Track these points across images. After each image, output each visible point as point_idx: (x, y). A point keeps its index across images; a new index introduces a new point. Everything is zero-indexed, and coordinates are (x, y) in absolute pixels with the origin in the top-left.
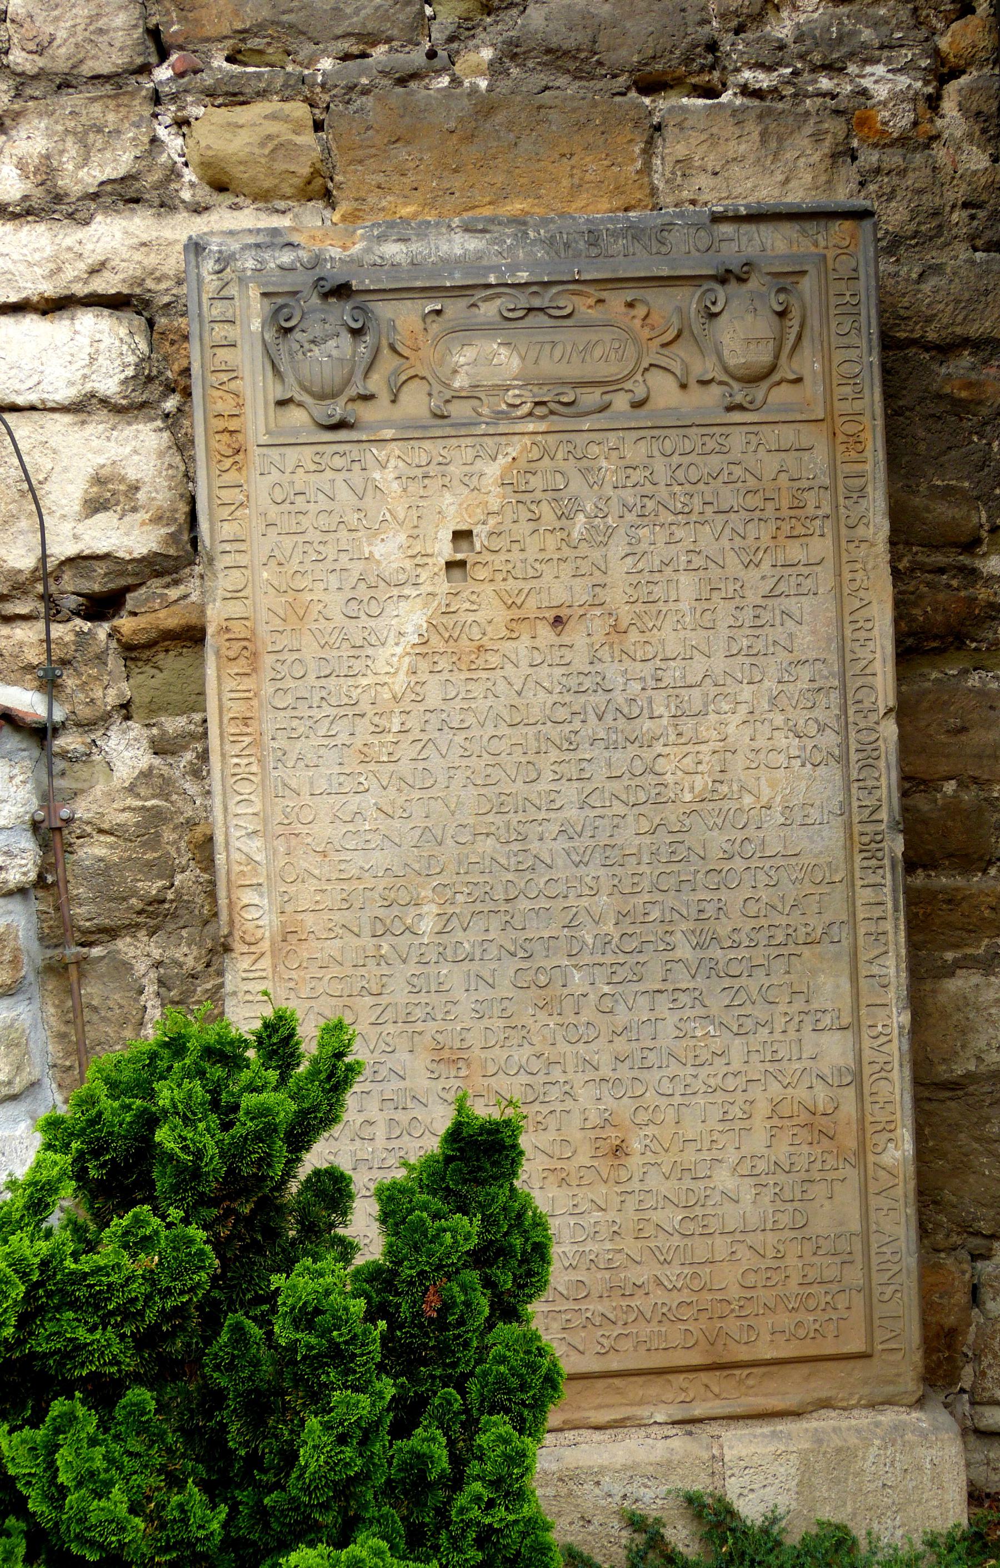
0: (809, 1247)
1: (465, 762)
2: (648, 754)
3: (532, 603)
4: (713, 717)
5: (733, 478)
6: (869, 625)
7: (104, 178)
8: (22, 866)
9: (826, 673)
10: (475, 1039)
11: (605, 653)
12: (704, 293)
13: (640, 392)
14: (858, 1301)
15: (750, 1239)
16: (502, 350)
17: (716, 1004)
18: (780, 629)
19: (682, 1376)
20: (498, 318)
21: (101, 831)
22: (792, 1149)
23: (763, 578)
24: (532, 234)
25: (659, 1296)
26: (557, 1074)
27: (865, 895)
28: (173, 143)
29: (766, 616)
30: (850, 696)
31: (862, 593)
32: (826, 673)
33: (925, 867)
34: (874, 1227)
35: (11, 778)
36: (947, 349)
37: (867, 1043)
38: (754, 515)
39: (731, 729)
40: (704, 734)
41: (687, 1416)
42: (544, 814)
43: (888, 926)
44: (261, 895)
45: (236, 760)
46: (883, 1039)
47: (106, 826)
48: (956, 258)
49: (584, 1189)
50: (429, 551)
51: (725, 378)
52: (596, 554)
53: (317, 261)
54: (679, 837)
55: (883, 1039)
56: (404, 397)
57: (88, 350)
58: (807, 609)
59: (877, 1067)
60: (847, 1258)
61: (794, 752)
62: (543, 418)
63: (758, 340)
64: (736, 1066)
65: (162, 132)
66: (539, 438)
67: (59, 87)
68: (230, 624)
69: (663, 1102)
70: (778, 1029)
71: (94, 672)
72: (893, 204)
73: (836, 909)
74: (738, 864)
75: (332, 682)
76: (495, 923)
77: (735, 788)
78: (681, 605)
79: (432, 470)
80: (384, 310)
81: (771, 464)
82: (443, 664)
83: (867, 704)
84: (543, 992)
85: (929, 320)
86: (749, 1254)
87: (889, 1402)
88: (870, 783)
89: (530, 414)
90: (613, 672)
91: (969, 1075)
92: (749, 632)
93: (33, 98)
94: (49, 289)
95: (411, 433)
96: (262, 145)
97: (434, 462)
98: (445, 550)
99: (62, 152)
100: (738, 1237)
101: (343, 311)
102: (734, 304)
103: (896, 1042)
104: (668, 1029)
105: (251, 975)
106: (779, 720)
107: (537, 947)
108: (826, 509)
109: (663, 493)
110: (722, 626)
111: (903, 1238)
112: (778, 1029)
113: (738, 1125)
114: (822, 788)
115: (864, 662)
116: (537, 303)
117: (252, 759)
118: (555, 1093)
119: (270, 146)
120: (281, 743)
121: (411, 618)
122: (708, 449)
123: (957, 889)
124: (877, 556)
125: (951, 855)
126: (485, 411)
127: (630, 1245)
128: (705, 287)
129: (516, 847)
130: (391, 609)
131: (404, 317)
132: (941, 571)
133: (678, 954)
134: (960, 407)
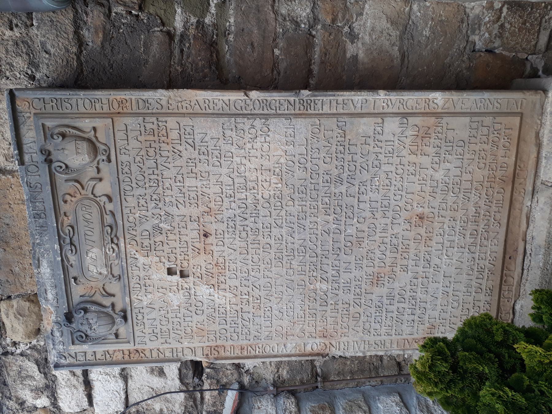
0: (473, 140)
1: (262, 272)
2: (262, 201)
3: (197, 245)
4: (247, 174)
5: (141, 161)
6: (207, 101)
7: (38, 372)
8: (290, 404)
9: (228, 124)
10: (370, 270)
11: (219, 217)
12: (57, 171)
13: (105, 199)
14: (498, 119)
15: (465, 165)
16: (90, 255)
17: (366, 176)
18: (209, 143)
19: (514, 193)
20: (76, 255)
21: (278, 371)
22: (431, 146)
23: (186, 150)
24: (38, 241)
25: (482, 203)
26: (387, 240)
27: (326, 109)
28: (22, 347)
29: (203, 149)
30: (238, 112)
31: (192, 104)
32: (228, 124)
33: (310, 65)
34: (469, 111)
35: (259, 408)
36: (81, 42)
37: (390, 110)
38: (158, 152)
39: (252, 167)
40: (254, 178)
41: (531, 193)
42: (284, 242)
43: (340, 99)
44: (308, 343)
45: (257, 352)
46: (389, 103)
47: (276, 370)
48: (37, 35)
49: (435, 231)
50: (176, 284)
51: (96, 162)
52: (177, 219)
53: (57, 323)
54: (296, 189)
55: (389, 103)
56: (111, 291)
57: (104, 376)
58: (200, 131)
59: (401, 106)
60: (480, 123)
61: (263, 140)
62: (118, 239)
63: (77, 148)
64: (393, 169)
65: (18, 351)
66: (127, 241)
67: (5, 385)
68: (205, 354)
69: (404, 199)
70: (379, 150)
71: (221, 373)
72: (14, 64)
73: (331, 123)
74: (309, 165)
75: (228, 320)
76: (325, 261)
77: (277, 166)
78: (199, 186)
79: (142, 283)
80: (76, 299)
81: (134, 144)
82: (222, 279)
83: (243, 104)
84: (354, 244)
85: (67, 51)
86: (471, 166)
87: (542, 107)
88: (278, 105)
89: (117, 244)
90: (227, 214)
91: (399, 50)
92: (210, 157)
93: (10, 394)
94: (81, 388)
95: (127, 290)
96: (19, 319)
97: (139, 282)
98: (176, 278)
99: (30, 385)
100: (464, 170)
101: (78, 316)
102: (61, 158)
103: (391, 97)
104: (374, 196)
105: (338, 347)
106: (249, 146)
107: (336, 246)
108: (154, 119)
109: (149, 191)
110: (208, 169)
111: (475, 97)
112: (379, 150)
113: (418, 169)
114: (278, 126)
115: (224, 105)
116: (68, 240)
117: (257, 346)
118: (395, 241)
119: (19, 316)
120: (251, 337)
121: (203, 291)
122: (129, 172)
123: (321, 51)
124: (175, 96)
125: (306, 53)
126: (116, 262)
127: (459, 215)
128: (54, 171)
129: (296, 253)
130: (200, 298)
131: (78, 291)
132: (182, 51)
133: (344, 191)
134: (107, 38)
